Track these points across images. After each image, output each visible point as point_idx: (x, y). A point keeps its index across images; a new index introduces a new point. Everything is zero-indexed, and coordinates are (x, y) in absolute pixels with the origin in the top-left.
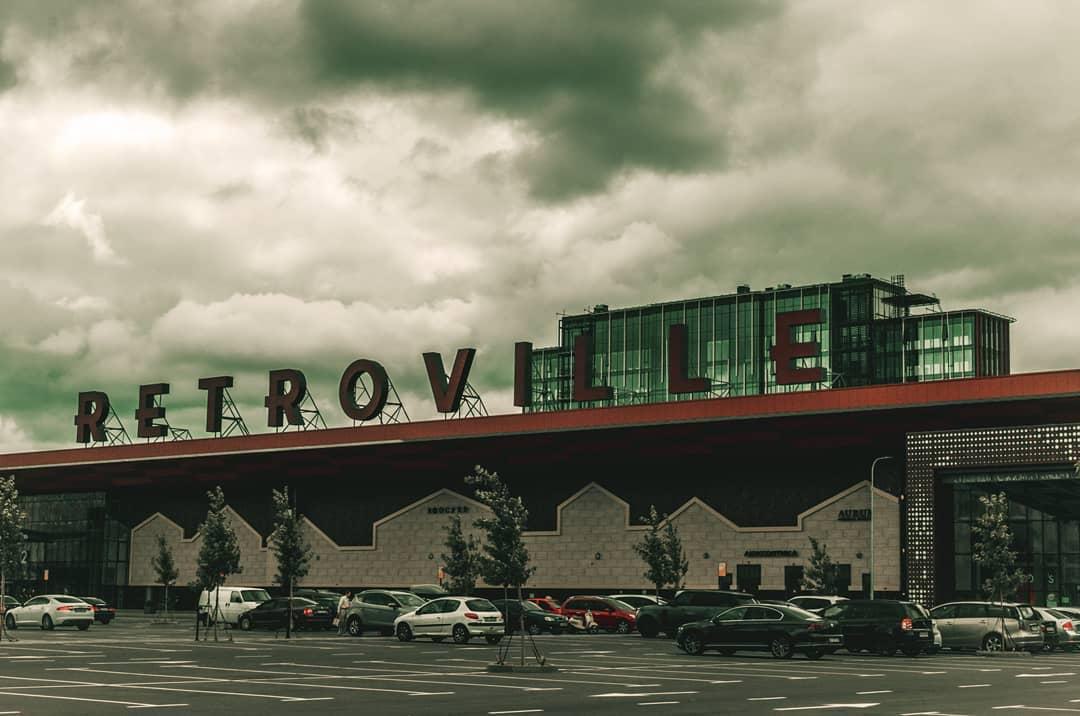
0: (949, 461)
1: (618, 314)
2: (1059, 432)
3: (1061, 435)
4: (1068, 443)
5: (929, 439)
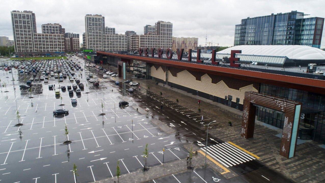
0: (254, 102)
1: (251, 19)
2: (280, 102)
3: (281, 103)
4: (282, 106)
5: (250, 95)
